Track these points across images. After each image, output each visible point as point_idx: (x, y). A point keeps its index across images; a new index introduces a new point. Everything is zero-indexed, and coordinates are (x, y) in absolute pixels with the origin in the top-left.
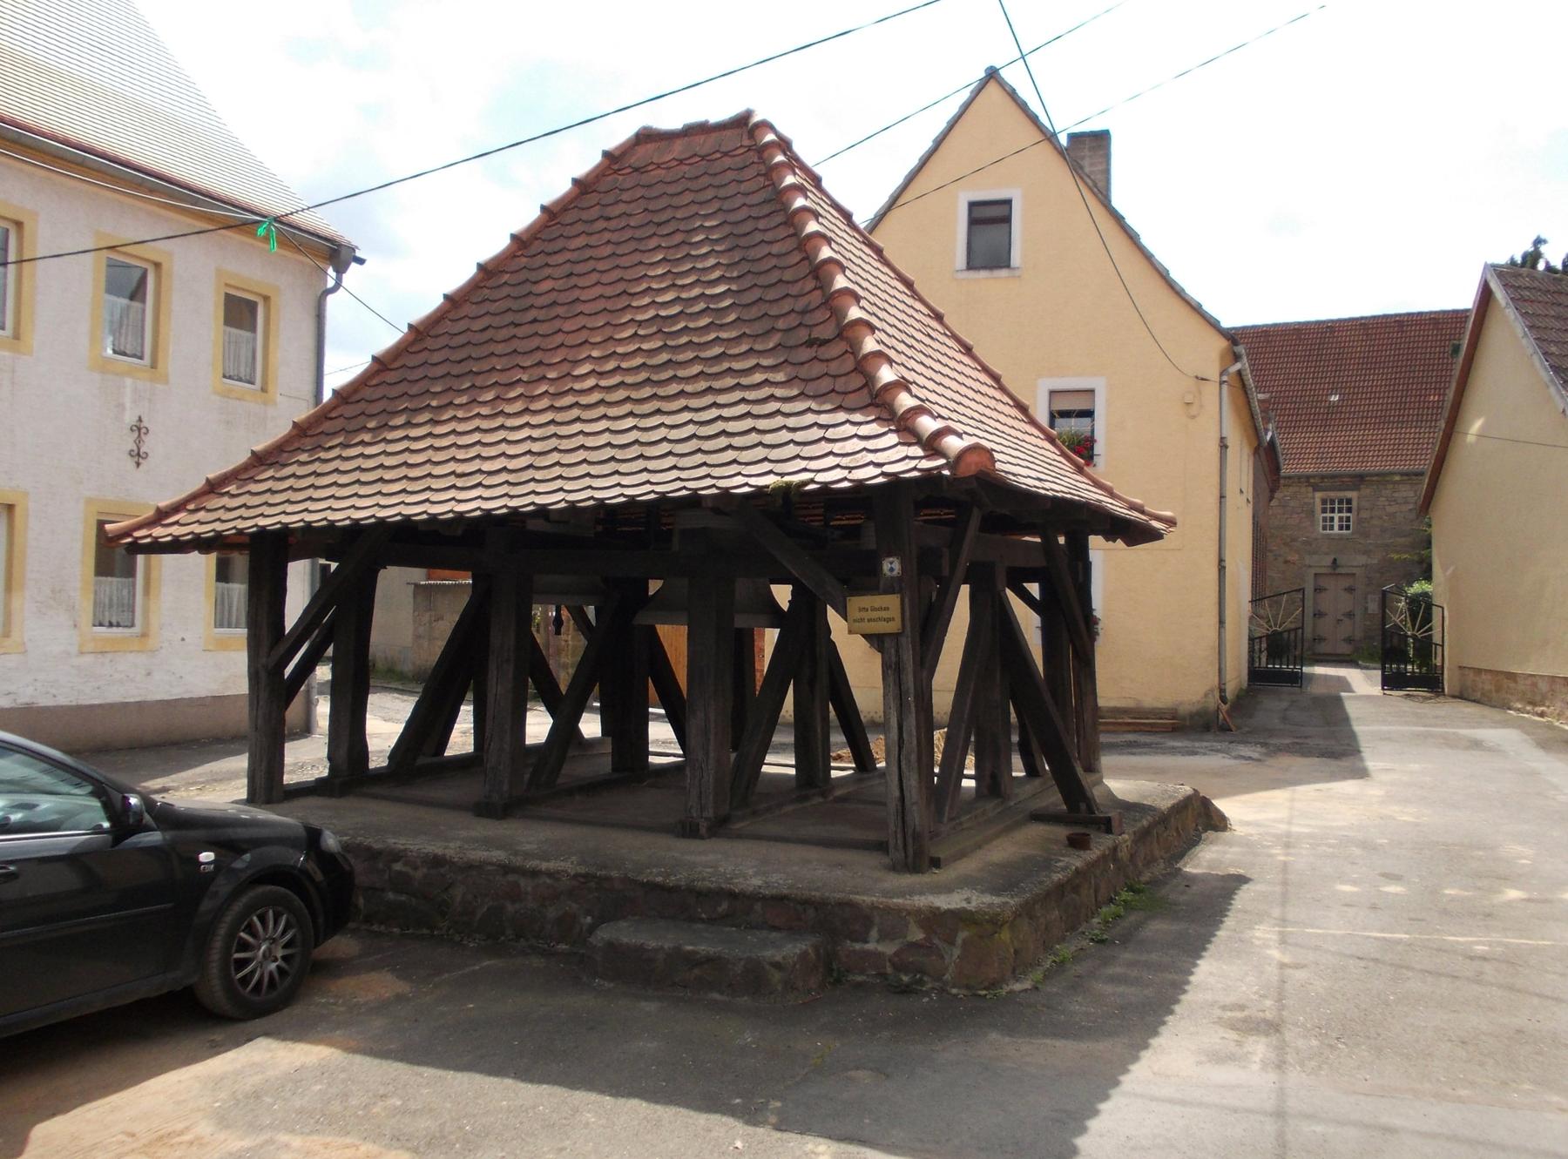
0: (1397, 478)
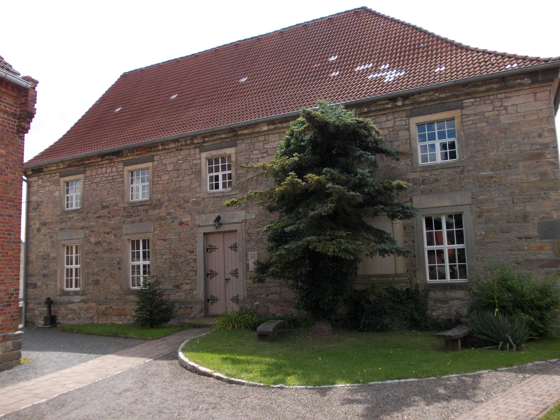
0: (265, 128)
